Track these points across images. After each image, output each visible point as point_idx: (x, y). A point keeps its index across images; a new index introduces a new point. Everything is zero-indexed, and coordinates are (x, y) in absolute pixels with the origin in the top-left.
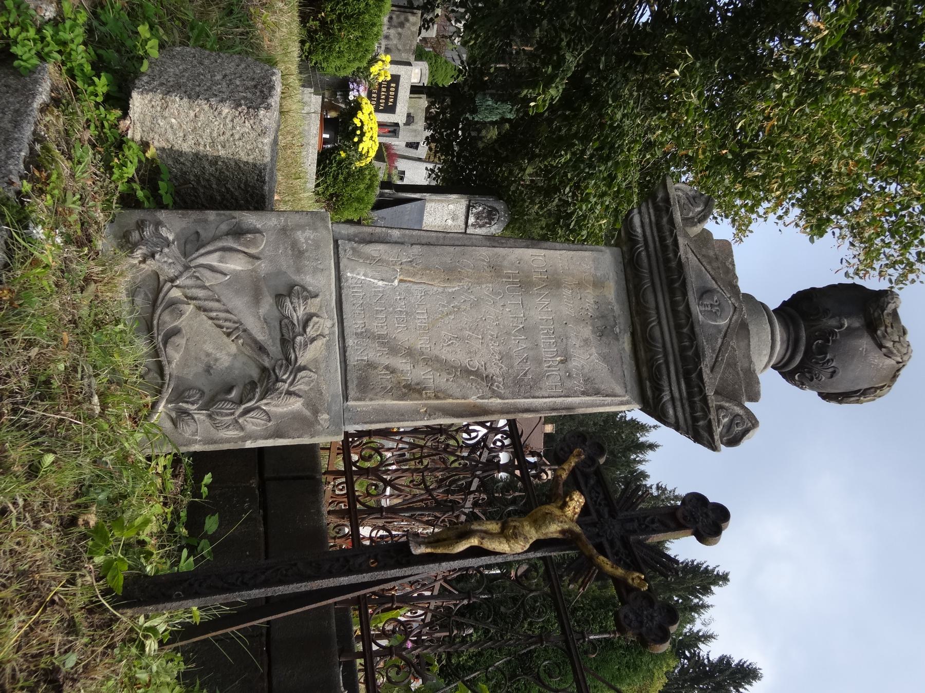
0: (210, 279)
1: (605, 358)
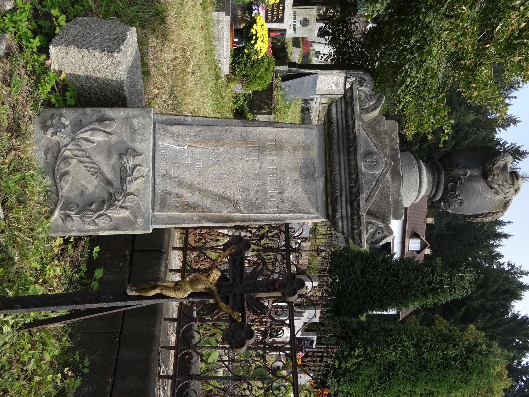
0: (85, 145)
1: (306, 191)
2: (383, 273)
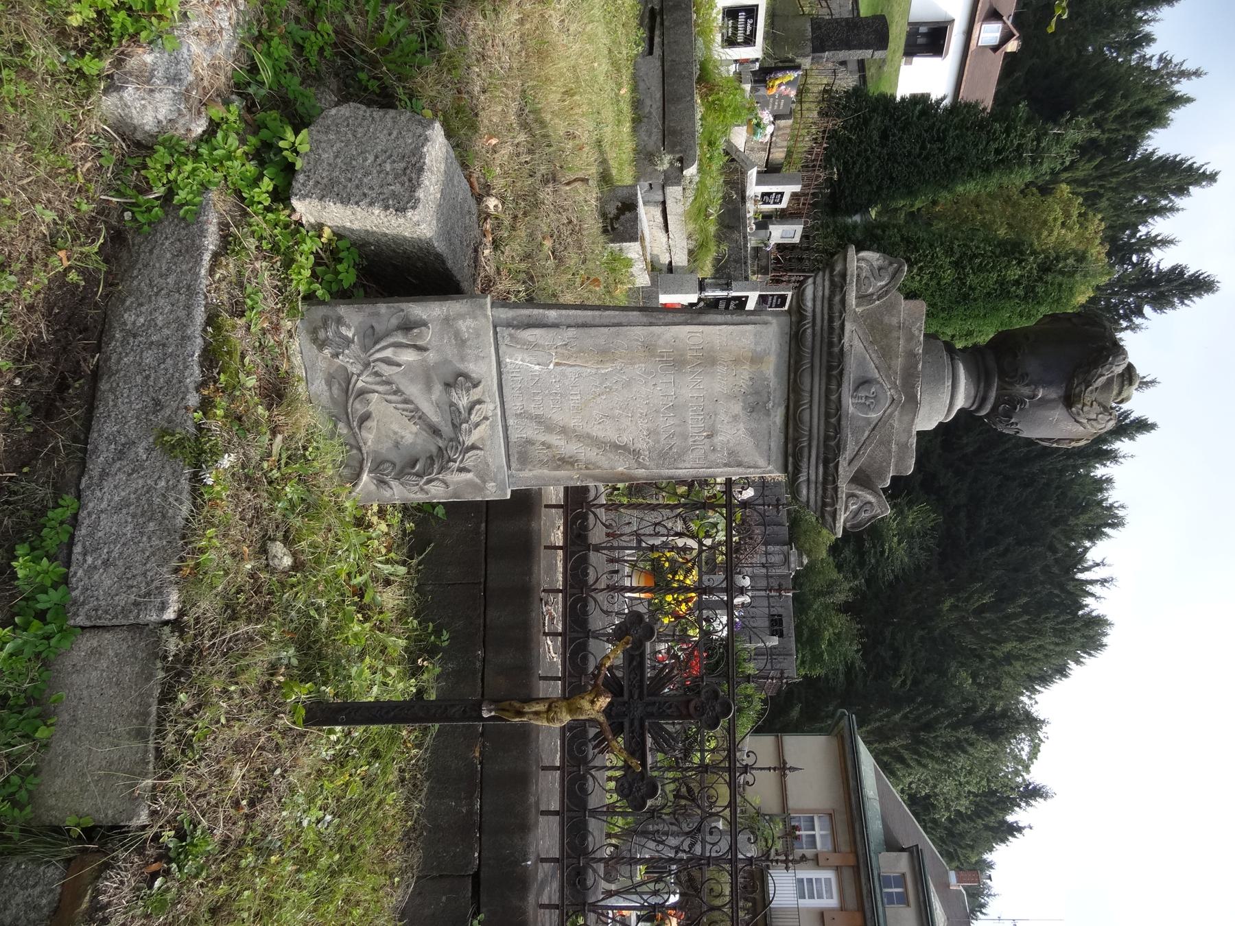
1: (752, 433)
2: (919, 136)
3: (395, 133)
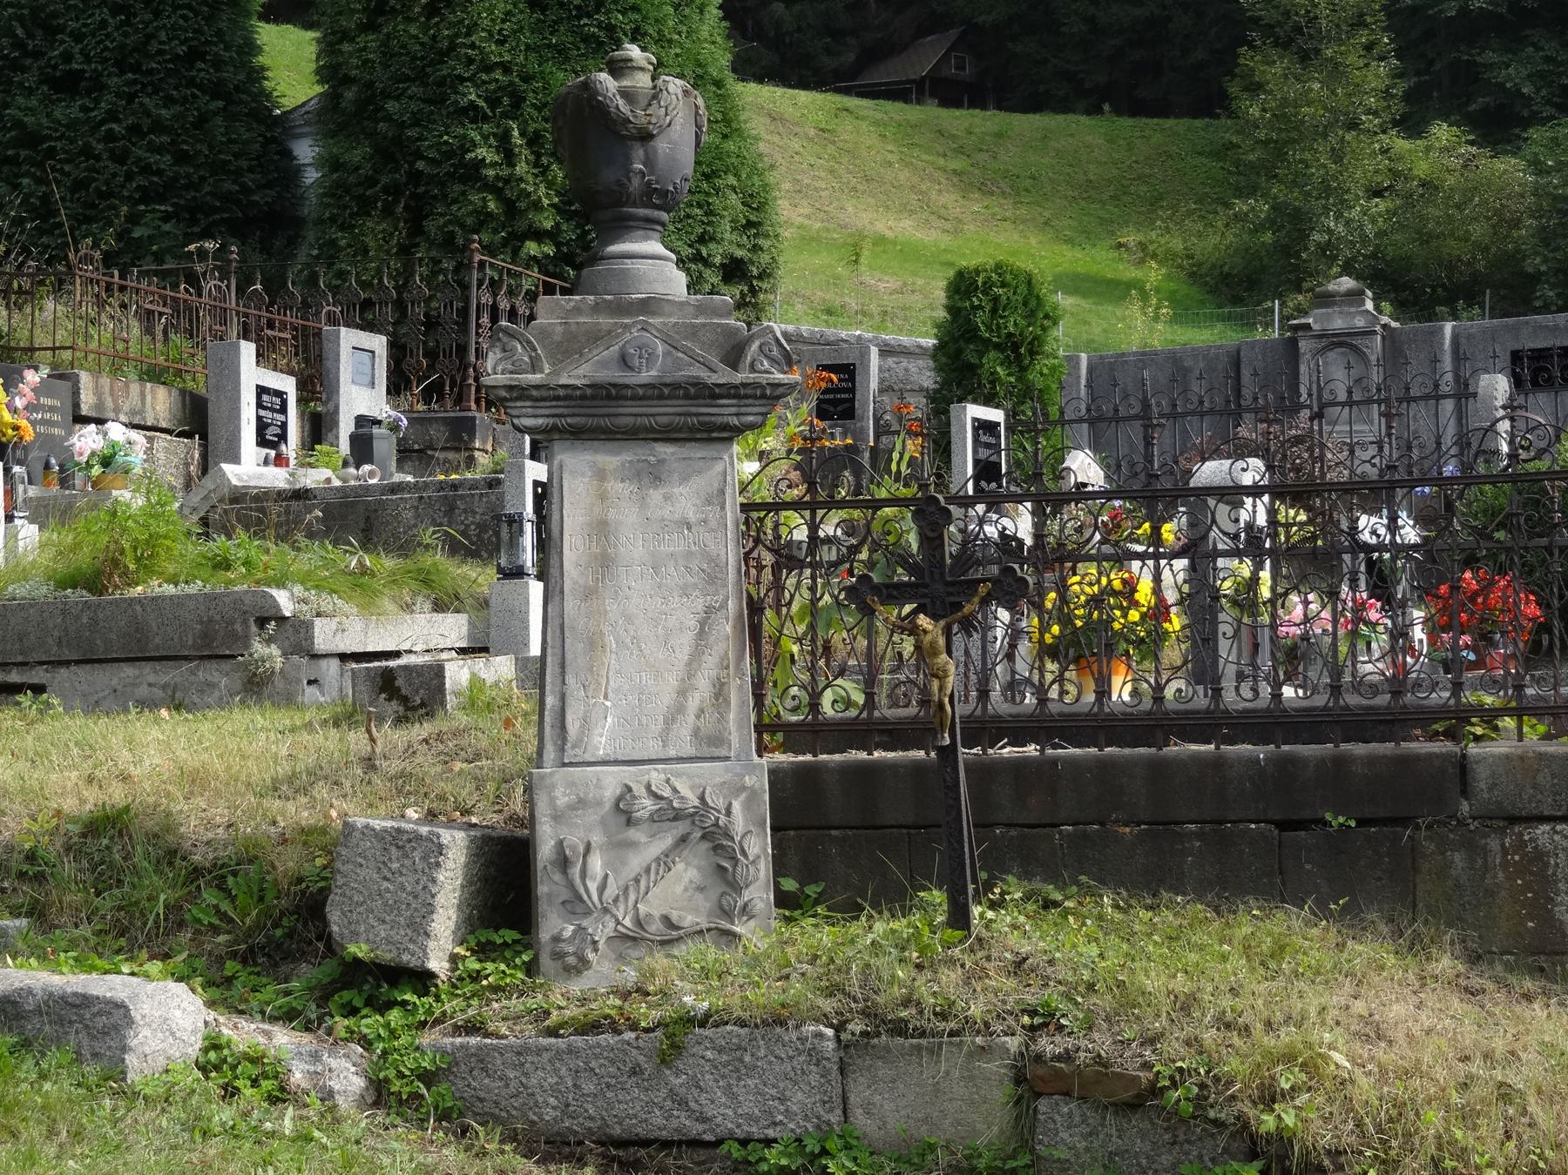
0: (612, 890)
1: (685, 479)
3: (360, 860)
